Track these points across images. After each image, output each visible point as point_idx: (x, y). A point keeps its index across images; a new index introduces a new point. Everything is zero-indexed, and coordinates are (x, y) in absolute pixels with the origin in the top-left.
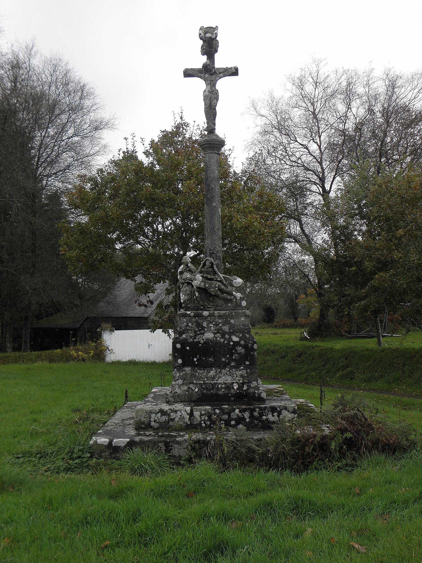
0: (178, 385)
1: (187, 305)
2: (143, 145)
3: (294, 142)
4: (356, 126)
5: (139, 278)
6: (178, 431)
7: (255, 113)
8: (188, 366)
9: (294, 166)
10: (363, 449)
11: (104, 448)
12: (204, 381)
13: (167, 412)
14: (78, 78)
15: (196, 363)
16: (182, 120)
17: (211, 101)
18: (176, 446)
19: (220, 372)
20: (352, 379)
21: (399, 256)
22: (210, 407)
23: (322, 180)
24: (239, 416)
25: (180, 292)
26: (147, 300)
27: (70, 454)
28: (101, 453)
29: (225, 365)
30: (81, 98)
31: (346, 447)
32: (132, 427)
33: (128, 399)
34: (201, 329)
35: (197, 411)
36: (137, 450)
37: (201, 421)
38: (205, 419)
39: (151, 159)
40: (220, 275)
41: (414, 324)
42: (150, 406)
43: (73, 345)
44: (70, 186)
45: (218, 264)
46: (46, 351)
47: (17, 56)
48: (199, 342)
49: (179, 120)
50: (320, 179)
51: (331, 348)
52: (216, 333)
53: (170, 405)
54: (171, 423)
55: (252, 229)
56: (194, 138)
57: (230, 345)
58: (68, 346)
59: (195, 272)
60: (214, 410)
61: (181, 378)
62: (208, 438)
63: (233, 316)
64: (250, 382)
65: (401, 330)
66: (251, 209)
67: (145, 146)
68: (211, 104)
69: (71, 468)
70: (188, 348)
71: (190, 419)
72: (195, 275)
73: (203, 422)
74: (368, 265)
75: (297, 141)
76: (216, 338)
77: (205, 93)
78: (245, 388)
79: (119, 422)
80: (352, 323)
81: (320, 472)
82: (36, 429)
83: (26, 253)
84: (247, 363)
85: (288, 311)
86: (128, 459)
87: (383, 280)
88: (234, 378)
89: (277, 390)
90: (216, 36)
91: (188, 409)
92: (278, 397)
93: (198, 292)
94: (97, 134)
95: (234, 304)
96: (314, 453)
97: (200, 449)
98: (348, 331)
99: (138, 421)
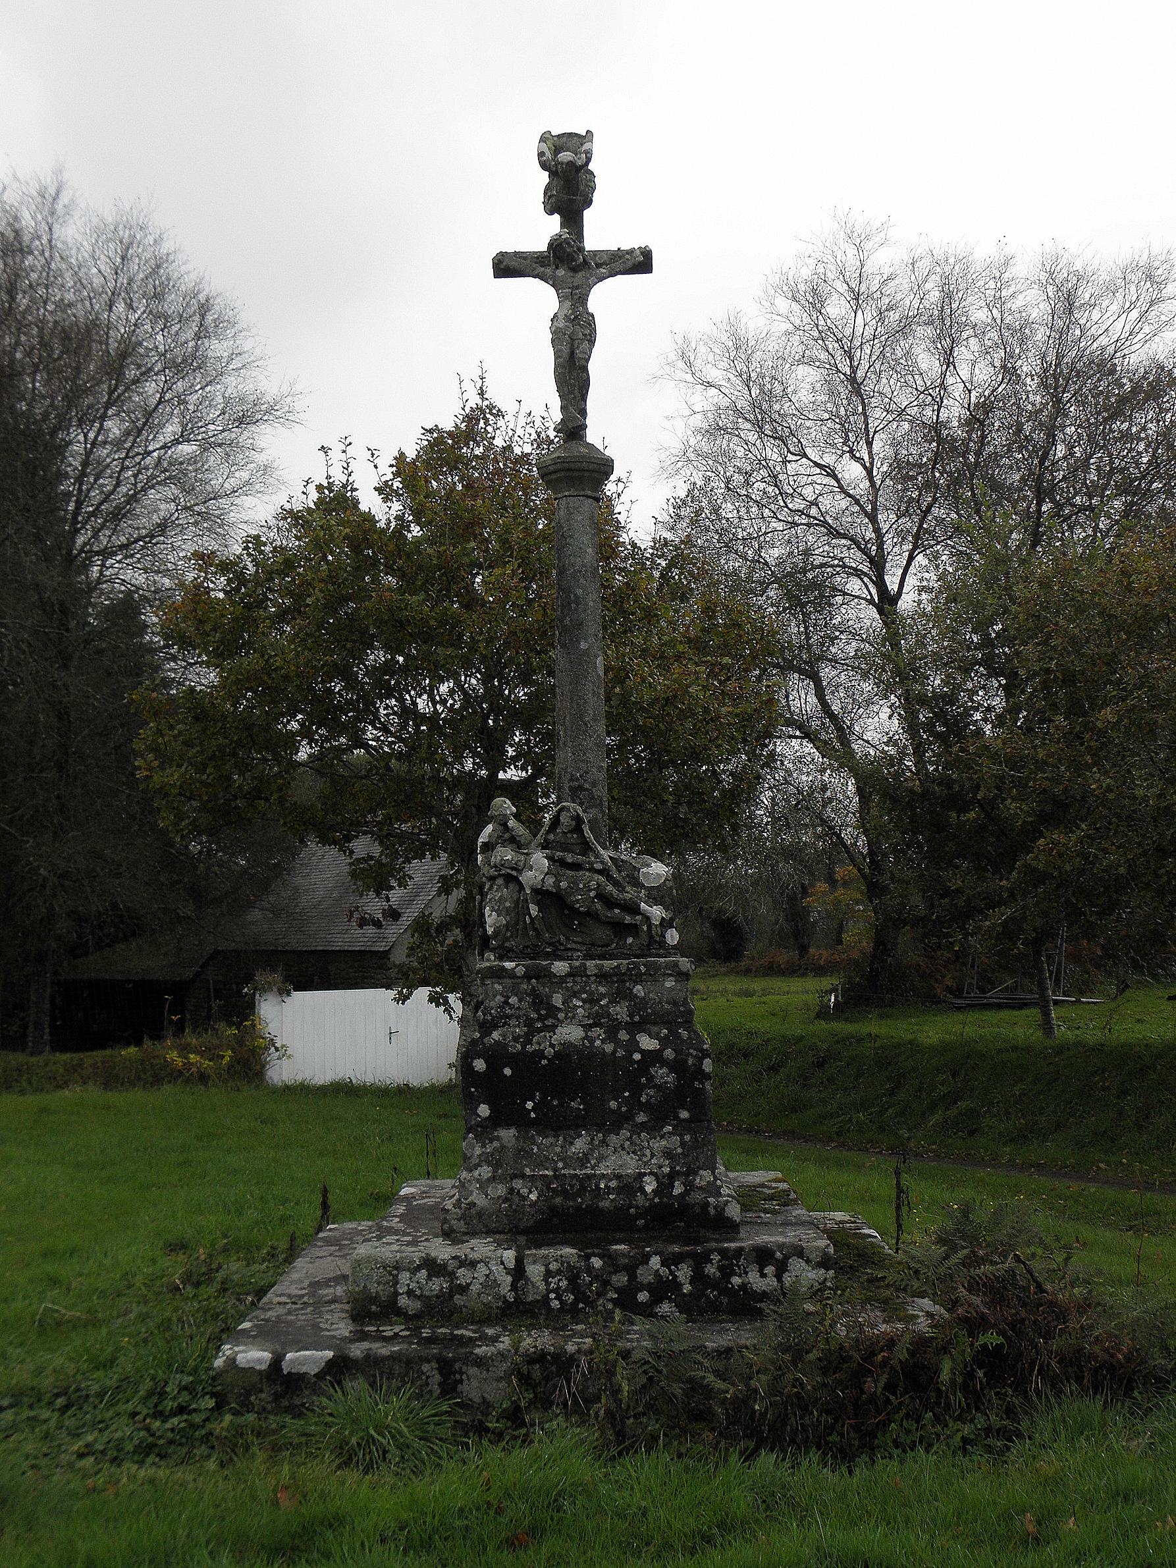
0: (478, 1181)
1: (504, 942)
2: (376, 467)
3: (799, 458)
4: (971, 414)
5: (364, 846)
6: (480, 1322)
7: (689, 378)
8: (508, 1125)
9: (798, 525)
10: (1037, 1382)
11: (255, 1379)
12: (555, 1170)
13: (444, 1266)
14: (193, 276)
15: (533, 1115)
16: (483, 399)
17: (573, 345)
18: (473, 1371)
19: (604, 1142)
20: (972, 1132)
21: (1104, 785)
22: (574, 1251)
23: (878, 564)
24: (661, 1277)
25: (482, 901)
26: (384, 910)
27: (155, 1399)
28: (248, 1393)
29: (618, 1122)
30: (198, 337)
31: (985, 1374)
32: (342, 1311)
33: (331, 1213)
34: (548, 1016)
35: (535, 1262)
36: (355, 1384)
37: (549, 1291)
38: (559, 1288)
39: (396, 506)
40: (602, 852)
41: (1136, 967)
42: (395, 1247)
43: (174, 1035)
44: (167, 582)
45: (596, 819)
46: (95, 1053)
47: (16, 218)
48: (540, 1054)
49: (474, 400)
50: (872, 560)
51: (910, 1042)
52: (591, 1026)
53: (455, 1242)
54: (458, 1300)
55: (684, 704)
56: (517, 451)
57: (633, 1062)
58: (157, 1036)
59: (527, 846)
60: (587, 1257)
61: (487, 1159)
62: (571, 1348)
63: (642, 974)
64: (692, 1172)
65: (1102, 983)
66: (681, 648)
67: (381, 471)
68: (572, 353)
69: (156, 1445)
70: (507, 1072)
71: (514, 1287)
72: (527, 854)
73: (552, 1296)
74: (1014, 808)
75: (805, 456)
76: (592, 1041)
77: (555, 324)
78: (678, 1189)
79: (304, 1292)
80: (965, 964)
81: (910, 1454)
82: (57, 1311)
83: (41, 771)
84: (684, 1114)
85: (781, 927)
86: (331, 1415)
87: (1060, 855)
88: (645, 1159)
89: (770, 1188)
90: (589, 160)
91: (509, 1255)
92: (774, 1212)
93: (538, 903)
94: (243, 437)
95: (644, 939)
96: (892, 1397)
97: (547, 1379)
98: (955, 988)
99: (358, 1293)
